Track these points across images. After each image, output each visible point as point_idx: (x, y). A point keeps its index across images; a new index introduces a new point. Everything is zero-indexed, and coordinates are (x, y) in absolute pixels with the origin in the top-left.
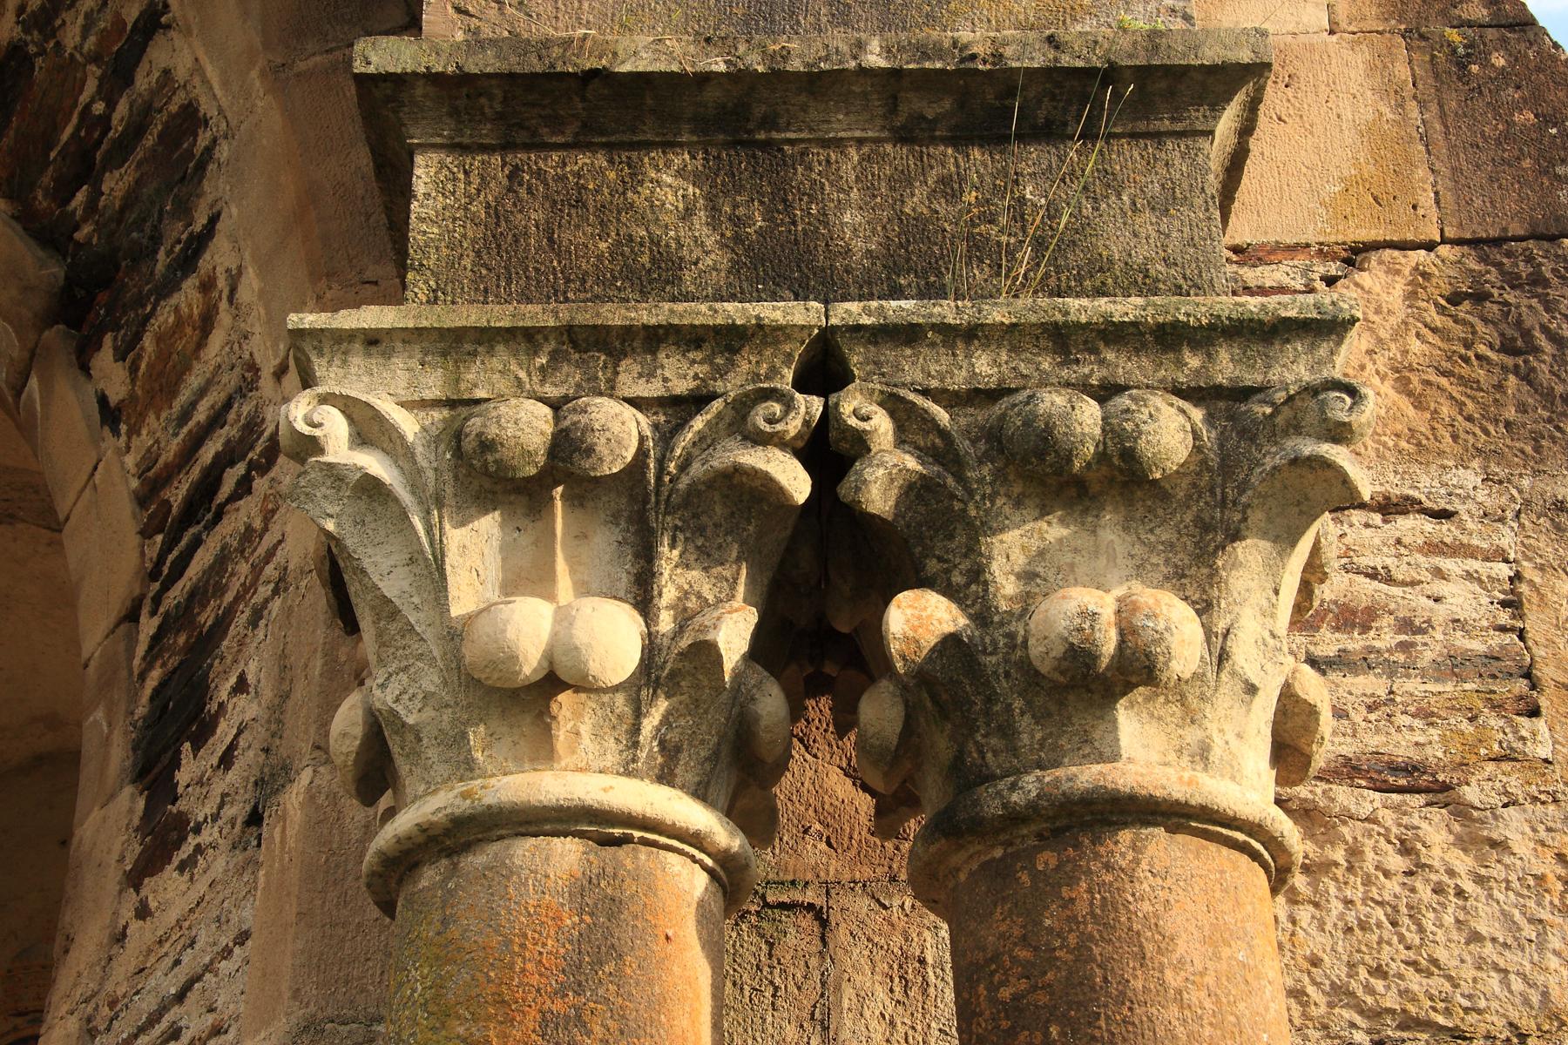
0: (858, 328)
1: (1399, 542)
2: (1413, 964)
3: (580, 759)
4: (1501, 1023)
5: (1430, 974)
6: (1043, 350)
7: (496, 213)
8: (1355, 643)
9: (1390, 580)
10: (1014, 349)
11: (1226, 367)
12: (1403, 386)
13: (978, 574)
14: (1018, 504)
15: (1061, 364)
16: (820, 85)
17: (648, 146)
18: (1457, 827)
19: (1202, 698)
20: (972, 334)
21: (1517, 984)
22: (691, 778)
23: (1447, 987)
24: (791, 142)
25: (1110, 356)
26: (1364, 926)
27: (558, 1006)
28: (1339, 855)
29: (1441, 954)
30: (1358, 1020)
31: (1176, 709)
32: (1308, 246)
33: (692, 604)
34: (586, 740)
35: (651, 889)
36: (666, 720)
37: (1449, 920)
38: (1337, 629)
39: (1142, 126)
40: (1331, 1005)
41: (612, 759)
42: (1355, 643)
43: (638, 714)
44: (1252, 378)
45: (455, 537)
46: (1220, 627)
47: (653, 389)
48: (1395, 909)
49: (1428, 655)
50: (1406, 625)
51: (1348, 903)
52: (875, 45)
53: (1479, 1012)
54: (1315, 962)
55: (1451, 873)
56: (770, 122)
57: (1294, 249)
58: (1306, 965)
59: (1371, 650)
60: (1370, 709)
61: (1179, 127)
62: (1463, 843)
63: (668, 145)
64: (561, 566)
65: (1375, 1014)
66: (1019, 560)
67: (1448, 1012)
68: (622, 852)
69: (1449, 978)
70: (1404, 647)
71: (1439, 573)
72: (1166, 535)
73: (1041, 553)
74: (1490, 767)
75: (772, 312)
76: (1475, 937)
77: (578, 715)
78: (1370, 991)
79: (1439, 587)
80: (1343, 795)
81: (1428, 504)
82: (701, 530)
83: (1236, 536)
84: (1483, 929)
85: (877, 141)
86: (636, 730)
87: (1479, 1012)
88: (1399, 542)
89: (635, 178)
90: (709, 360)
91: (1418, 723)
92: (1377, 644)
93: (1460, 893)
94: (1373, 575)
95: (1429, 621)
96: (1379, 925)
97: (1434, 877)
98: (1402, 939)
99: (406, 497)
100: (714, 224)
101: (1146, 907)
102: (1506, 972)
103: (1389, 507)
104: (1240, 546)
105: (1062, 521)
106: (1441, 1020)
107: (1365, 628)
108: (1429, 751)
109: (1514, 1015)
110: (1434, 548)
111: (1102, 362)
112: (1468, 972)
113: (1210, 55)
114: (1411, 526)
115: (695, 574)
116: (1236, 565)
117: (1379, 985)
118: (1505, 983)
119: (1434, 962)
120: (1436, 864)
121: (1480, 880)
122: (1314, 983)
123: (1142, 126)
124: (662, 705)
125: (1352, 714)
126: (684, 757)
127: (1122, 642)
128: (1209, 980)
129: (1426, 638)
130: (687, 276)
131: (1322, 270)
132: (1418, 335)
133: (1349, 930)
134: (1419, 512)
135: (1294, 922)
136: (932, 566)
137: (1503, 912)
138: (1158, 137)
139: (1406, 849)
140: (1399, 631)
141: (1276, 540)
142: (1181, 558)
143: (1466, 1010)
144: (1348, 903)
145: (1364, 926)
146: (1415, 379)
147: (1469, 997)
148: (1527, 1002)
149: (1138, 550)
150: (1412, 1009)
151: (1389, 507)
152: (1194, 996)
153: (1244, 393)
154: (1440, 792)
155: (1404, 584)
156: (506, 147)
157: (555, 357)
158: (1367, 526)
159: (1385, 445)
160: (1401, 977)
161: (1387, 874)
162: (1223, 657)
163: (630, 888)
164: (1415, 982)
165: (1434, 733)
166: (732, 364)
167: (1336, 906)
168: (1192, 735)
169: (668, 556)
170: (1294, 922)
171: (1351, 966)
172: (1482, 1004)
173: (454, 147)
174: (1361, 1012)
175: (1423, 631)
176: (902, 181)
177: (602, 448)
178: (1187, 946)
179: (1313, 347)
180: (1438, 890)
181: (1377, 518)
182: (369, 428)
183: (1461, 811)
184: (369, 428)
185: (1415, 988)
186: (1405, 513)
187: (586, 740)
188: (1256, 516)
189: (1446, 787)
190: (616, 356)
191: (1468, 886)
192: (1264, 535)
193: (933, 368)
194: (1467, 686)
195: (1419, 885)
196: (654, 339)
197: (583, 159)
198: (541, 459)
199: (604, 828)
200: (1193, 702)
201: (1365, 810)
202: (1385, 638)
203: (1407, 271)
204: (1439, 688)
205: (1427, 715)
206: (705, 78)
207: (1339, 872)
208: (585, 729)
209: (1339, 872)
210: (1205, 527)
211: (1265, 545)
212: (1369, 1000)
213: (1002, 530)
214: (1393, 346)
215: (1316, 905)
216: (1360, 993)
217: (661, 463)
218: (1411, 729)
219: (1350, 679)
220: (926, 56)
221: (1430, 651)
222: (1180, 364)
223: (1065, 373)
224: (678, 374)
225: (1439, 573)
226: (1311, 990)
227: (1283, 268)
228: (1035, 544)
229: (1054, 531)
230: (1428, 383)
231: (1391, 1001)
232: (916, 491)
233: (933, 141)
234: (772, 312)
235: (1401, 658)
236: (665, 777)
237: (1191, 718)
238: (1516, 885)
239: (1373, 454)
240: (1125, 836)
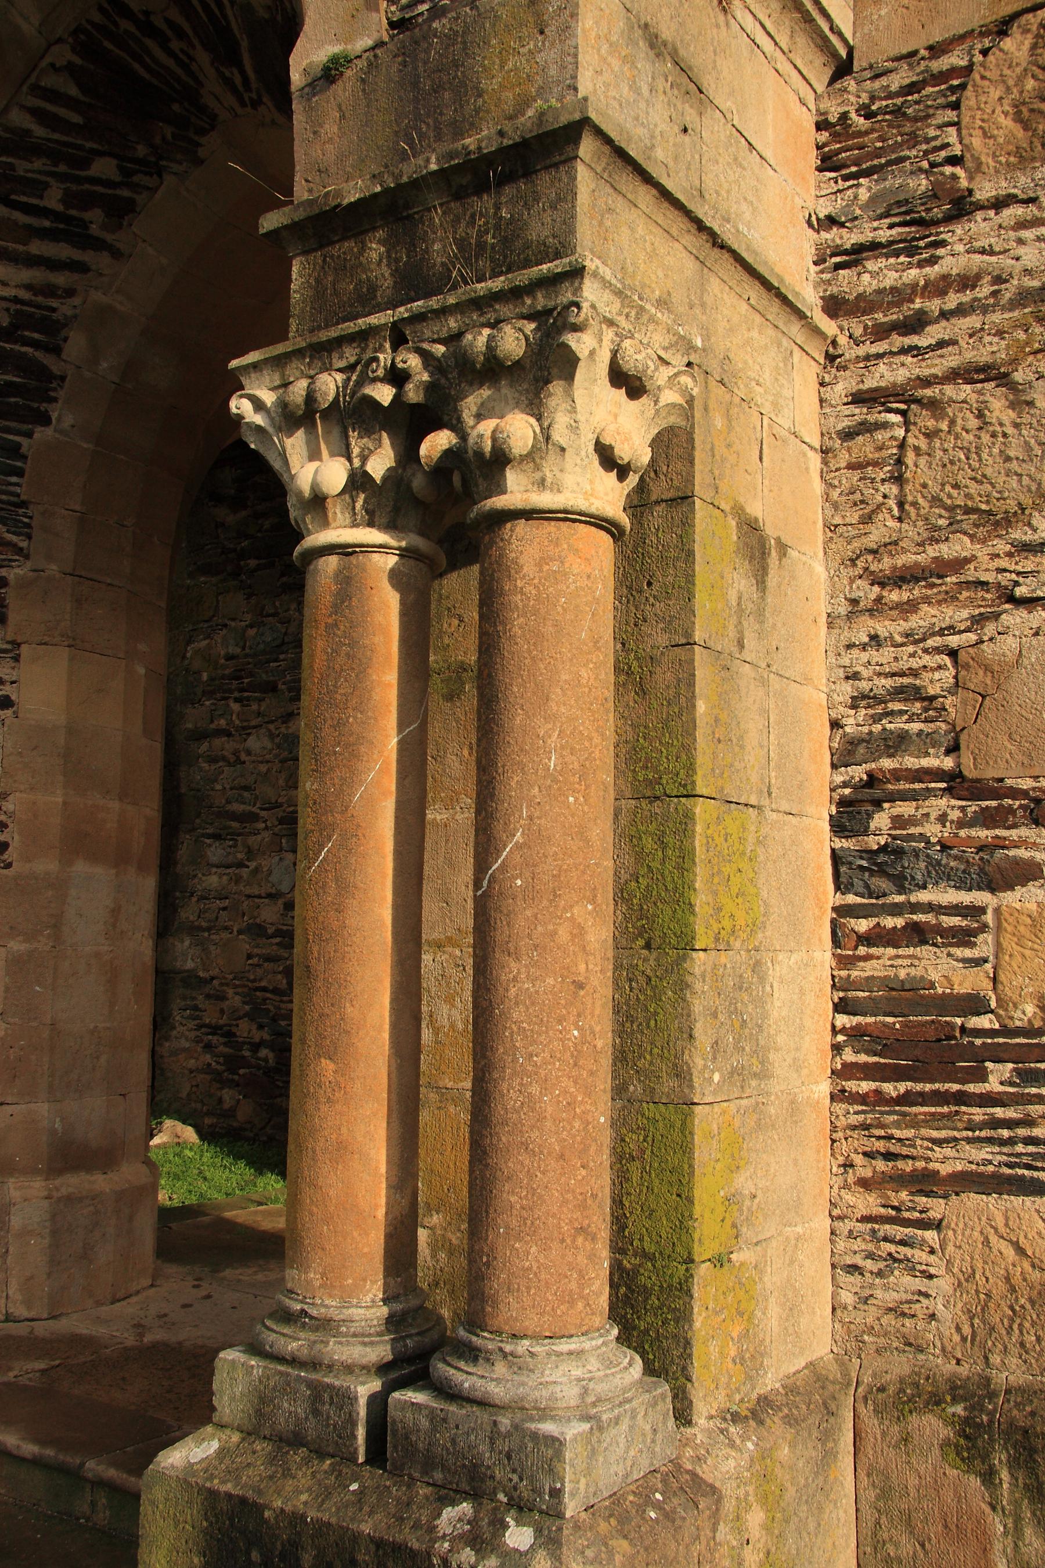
0: (404, 319)
1: (1000, 226)
2: (974, 479)
3: (338, 524)
4: (1013, 503)
5: (982, 483)
6: (472, 311)
7: (318, 281)
8: (967, 297)
9: (992, 253)
10: (462, 313)
11: (541, 301)
12: (1018, 118)
13: (459, 419)
14: (471, 384)
15: (480, 316)
16: (415, 184)
17: (366, 232)
18: (1011, 397)
19: (541, 458)
20: (444, 312)
21: (1026, 480)
22: (384, 521)
23: (990, 487)
24: (417, 213)
25: (497, 307)
26: (952, 462)
27: (330, 621)
28: (944, 426)
29: (989, 471)
30: (943, 513)
31: (531, 465)
32: (973, 31)
33: (366, 452)
34: (339, 515)
35: (364, 570)
36: (365, 501)
37: (996, 451)
38: (958, 291)
39: (548, 162)
40: (931, 507)
41: (348, 521)
42: (967, 297)
43: (354, 502)
44: (551, 304)
45: (289, 442)
46: (546, 424)
47: (342, 364)
48: (969, 450)
49: (1008, 295)
50: (998, 280)
51: (945, 451)
52: (433, 159)
53: (1004, 499)
54: (924, 486)
55: (1001, 425)
56: (407, 207)
57: (961, 38)
58: (920, 488)
59: (975, 299)
60: (971, 336)
61: (563, 158)
62: (1012, 406)
63: (374, 229)
64: (323, 446)
65: (951, 509)
66: (474, 409)
67: (988, 502)
68: (351, 558)
69: (991, 484)
70: (994, 294)
71: (1021, 242)
72: (525, 386)
73: (482, 404)
74: (1030, 358)
75: (374, 320)
76: (1008, 459)
77: (335, 506)
78: (950, 496)
79: (1021, 251)
80: (949, 390)
81: (1022, 196)
82: (364, 421)
83: (548, 382)
84: (1012, 454)
85: (448, 202)
86: (354, 508)
87: (1004, 499)
88: (1000, 226)
89: (363, 248)
90: (359, 346)
91: (996, 339)
92: (979, 296)
93: (1005, 435)
94: (983, 252)
95: (1010, 275)
96: (959, 460)
97: (991, 429)
98: (970, 466)
99: (271, 430)
100: (388, 265)
101: (513, 555)
102: (1021, 475)
103: (999, 204)
104: (550, 386)
105: (489, 388)
106: (984, 507)
107: (973, 287)
108: (998, 355)
109: (1022, 498)
110: (1022, 225)
111: (495, 311)
112: (1002, 479)
113: (564, 119)
114: (1015, 212)
115: (365, 440)
116: (550, 395)
117: (954, 493)
118: (1020, 481)
119: (984, 476)
120: (994, 421)
121: (1016, 426)
122: (924, 497)
123: (548, 162)
124: (362, 496)
125: (960, 341)
126: (378, 514)
127: (493, 446)
128: (536, 581)
129: (1008, 285)
130: (379, 294)
131: (979, 46)
132: (1033, 76)
133: (945, 466)
134: (1017, 202)
135: (916, 466)
136: (446, 418)
137: (1026, 442)
138: (556, 165)
139: (980, 415)
140: (993, 284)
141: (566, 379)
142: (531, 396)
143: (998, 499)
144: (945, 451)
145: (952, 462)
146: (1024, 110)
147: (1000, 492)
148: (1029, 490)
149: (517, 395)
150: (970, 503)
151: (999, 204)
152: (528, 589)
153: (548, 312)
154: (1003, 379)
155: (1000, 253)
156: (321, 247)
157: (311, 357)
158: (985, 220)
159: (1000, 163)
160: (966, 487)
161: (967, 432)
162: (548, 438)
163: (355, 571)
164: (973, 488)
165: (1003, 343)
166: (367, 346)
167: (939, 454)
168: (538, 475)
169: (353, 435)
170: (916, 466)
171: (943, 485)
172: (1006, 494)
173: (305, 253)
174: (945, 509)
175: (1006, 281)
176: (457, 221)
177: (319, 399)
178: (529, 569)
179: (572, 284)
180: (994, 435)
181: (991, 213)
182: (258, 405)
183: (1012, 386)
184: (258, 405)
185: (972, 491)
186: (1008, 205)
187: (339, 515)
188: (555, 371)
189: (1006, 375)
190: (330, 352)
191: (1010, 430)
192: (560, 378)
193: (435, 329)
194: (1026, 310)
195: (983, 435)
196: (339, 342)
197: (346, 244)
198: (303, 407)
199: (344, 550)
200: (538, 460)
201: (962, 396)
202: (984, 290)
203: (1034, 28)
204: (1011, 315)
205: (1000, 333)
206: (375, 196)
207: (942, 435)
208: (338, 511)
209: (942, 435)
210: (536, 380)
211: (561, 382)
212: (949, 502)
213: (466, 397)
214: (1015, 90)
215: (929, 455)
216: (945, 499)
217: (345, 396)
218: (991, 344)
219: (962, 320)
220: (452, 158)
221: (1009, 292)
222: (524, 303)
223: (482, 319)
224: (350, 354)
225: (1021, 242)
226: (921, 501)
227: (956, 53)
228: (479, 401)
229: (485, 393)
230: (1032, 111)
231: (960, 502)
232: (430, 388)
233: (468, 196)
234: (374, 320)
235: (991, 301)
236: (371, 524)
237: (538, 468)
238: (1035, 424)
239: (992, 171)
240: (509, 525)
